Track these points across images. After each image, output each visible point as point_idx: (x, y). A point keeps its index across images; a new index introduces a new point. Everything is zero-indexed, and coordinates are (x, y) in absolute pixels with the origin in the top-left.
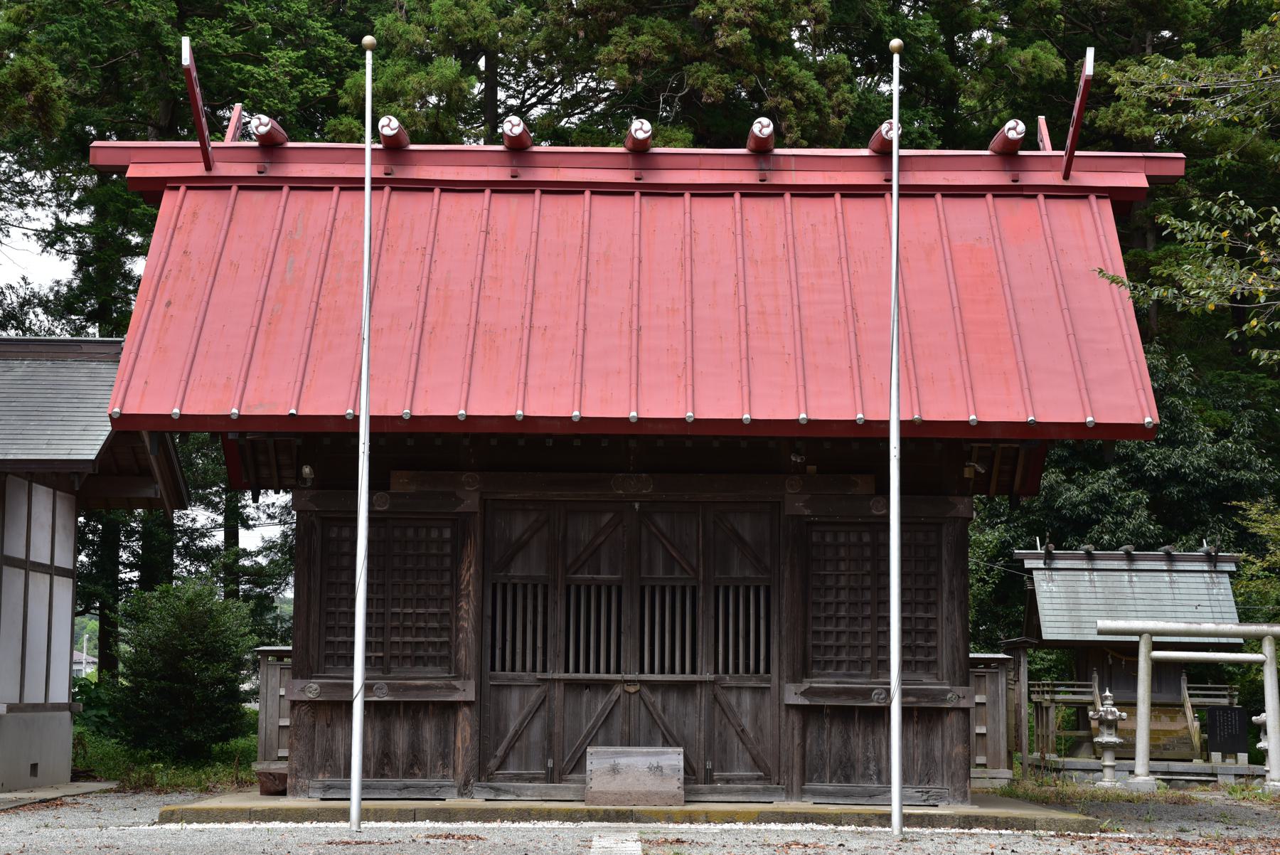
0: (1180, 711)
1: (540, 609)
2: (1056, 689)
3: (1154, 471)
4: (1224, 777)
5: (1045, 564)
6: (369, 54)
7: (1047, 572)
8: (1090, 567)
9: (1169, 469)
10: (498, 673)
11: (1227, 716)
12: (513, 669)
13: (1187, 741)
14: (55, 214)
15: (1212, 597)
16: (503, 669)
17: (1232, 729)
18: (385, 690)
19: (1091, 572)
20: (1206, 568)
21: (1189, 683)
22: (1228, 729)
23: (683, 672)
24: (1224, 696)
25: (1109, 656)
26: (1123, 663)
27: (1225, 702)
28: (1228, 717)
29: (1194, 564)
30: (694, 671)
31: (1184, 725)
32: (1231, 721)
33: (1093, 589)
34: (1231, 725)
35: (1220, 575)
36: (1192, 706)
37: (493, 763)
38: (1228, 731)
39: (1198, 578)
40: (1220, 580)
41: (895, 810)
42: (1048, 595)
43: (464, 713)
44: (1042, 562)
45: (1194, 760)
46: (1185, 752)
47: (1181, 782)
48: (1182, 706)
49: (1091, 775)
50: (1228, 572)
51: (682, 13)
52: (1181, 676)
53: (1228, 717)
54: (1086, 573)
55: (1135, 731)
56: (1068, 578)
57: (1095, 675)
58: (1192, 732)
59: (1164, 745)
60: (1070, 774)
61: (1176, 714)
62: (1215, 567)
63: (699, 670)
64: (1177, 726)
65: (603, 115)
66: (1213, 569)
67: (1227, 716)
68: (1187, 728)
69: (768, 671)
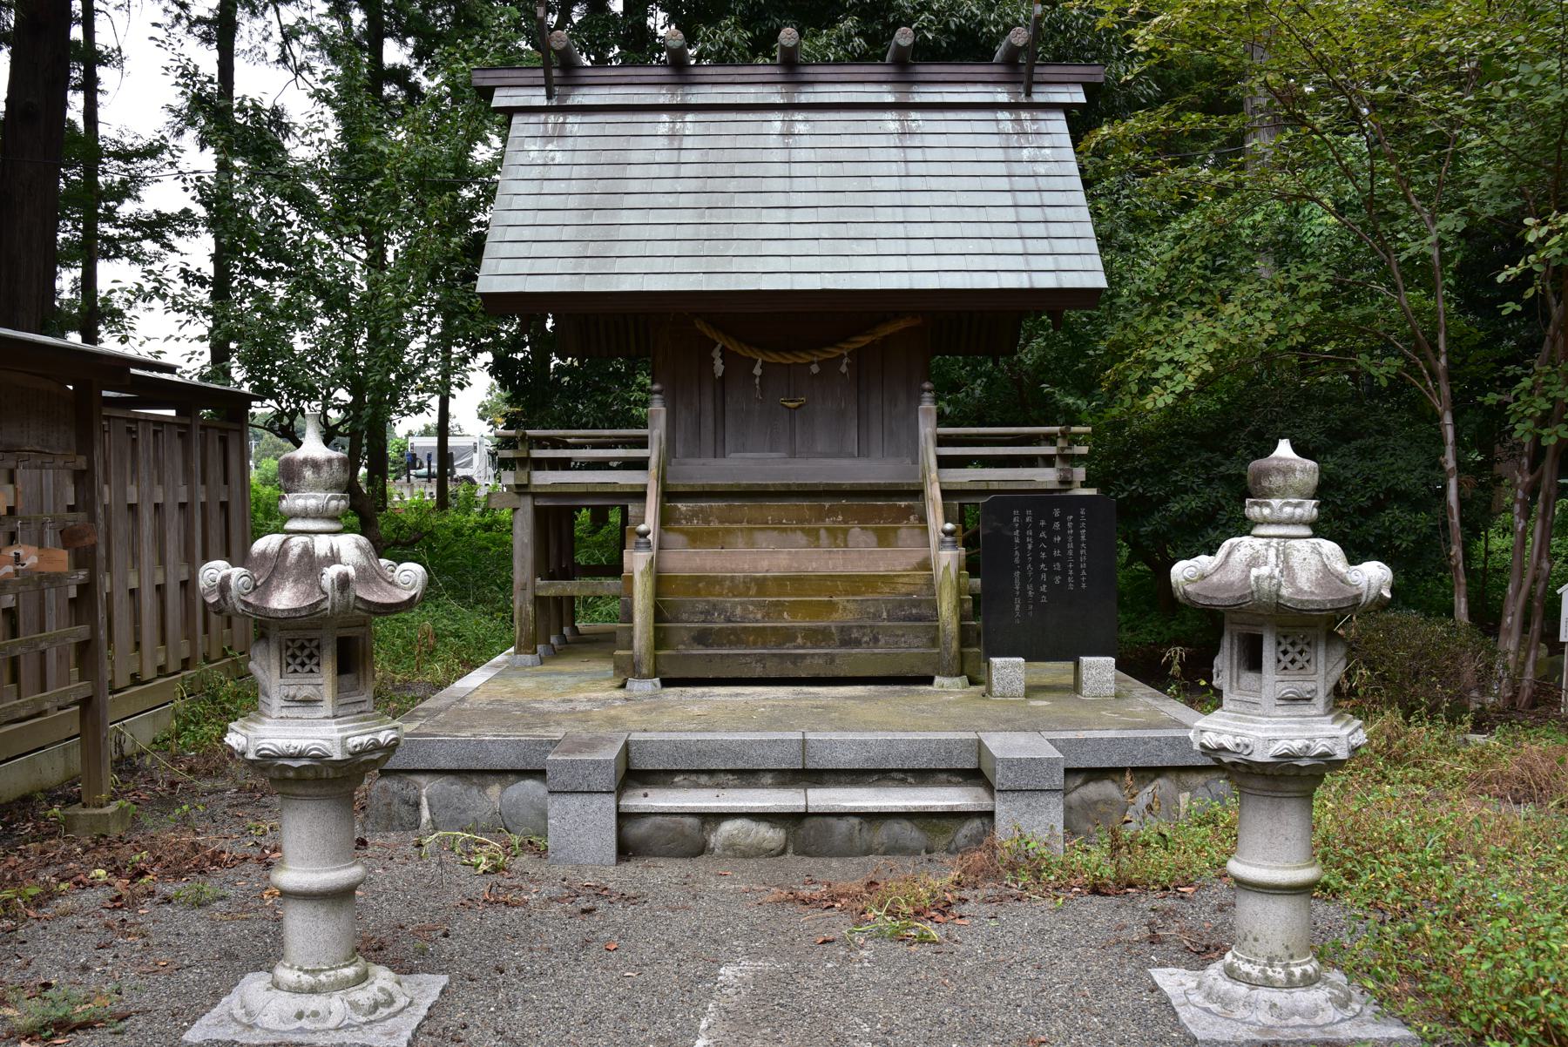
0: (908, 511)
2: (537, 453)
3: (930, 30)
4: (1021, 802)
5: (549, 97)
7: (552, 118)
8: (678, 100)
9: (959, 26)
11: (1048, 528)
13: (920, 612)
15: (1018, 169)
17: (1064, 573)
19: (677, 116)
20: (1003, 98)
21: (942, 420)
22: (1051, 573)
24: (1048, 461)
25: (716, 354)
26: (757, 371)
27: (1046, 477)
28: (1051, 533)
29: (971, 88)
31: (917, 556)
32: (1063, 546)
33: (673, 156)
34: (1063, 559)
35: (1041, 115)
36: (947, 494)
38: (1050, 582)
39: (979, 123)
40: (1042, 127)
42: (535, 172)
44: (543, 91)
45: (938, 679)
46: (909, 651)
47: (842, 826)
48: (917, 493)
49: (494, 790)
50: (1066, 108)
52: (919, 402)
53: (1051, 533)
54: (665, 117)
56: (609, 130)
57: (658, 410)
58: (939, 573)
59: (842, 629)
60: (410, 793)
61: (898, 520)
62: (1028, 94)
64: (893, 561)
66: (1023, 99)
67: (1048, 528)
68: (925, 565)
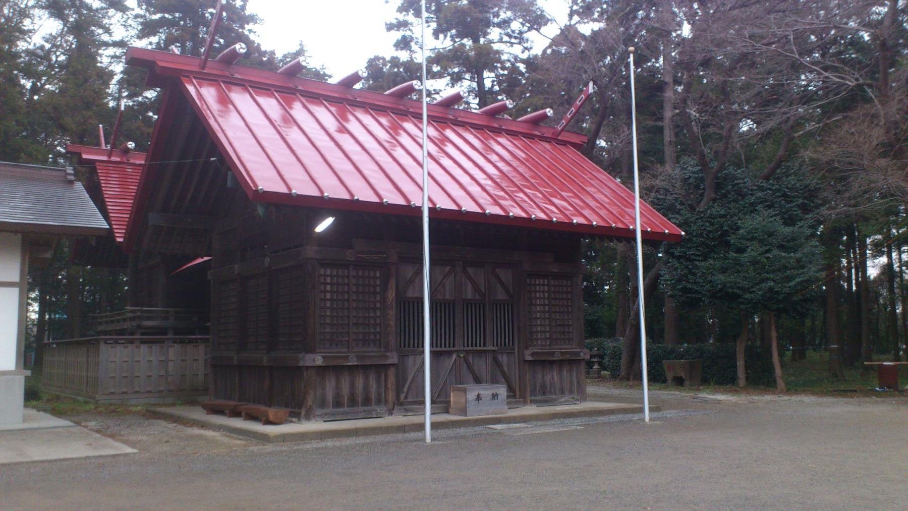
1: (506, 310)
6: (632, 55)
10: (407, 348)
12: (409, 347)
14: (413, 34)
16: (405, 347)
18: (355, 359)
23: (480, 346)
30: (484, 346)
37: (402, 396)
41: (428, 420)
43: (392, 372)
51: (9, 2)
55: (481, 383)
63: (487, 344)
65: (678, 114)
69: (513, 344)
